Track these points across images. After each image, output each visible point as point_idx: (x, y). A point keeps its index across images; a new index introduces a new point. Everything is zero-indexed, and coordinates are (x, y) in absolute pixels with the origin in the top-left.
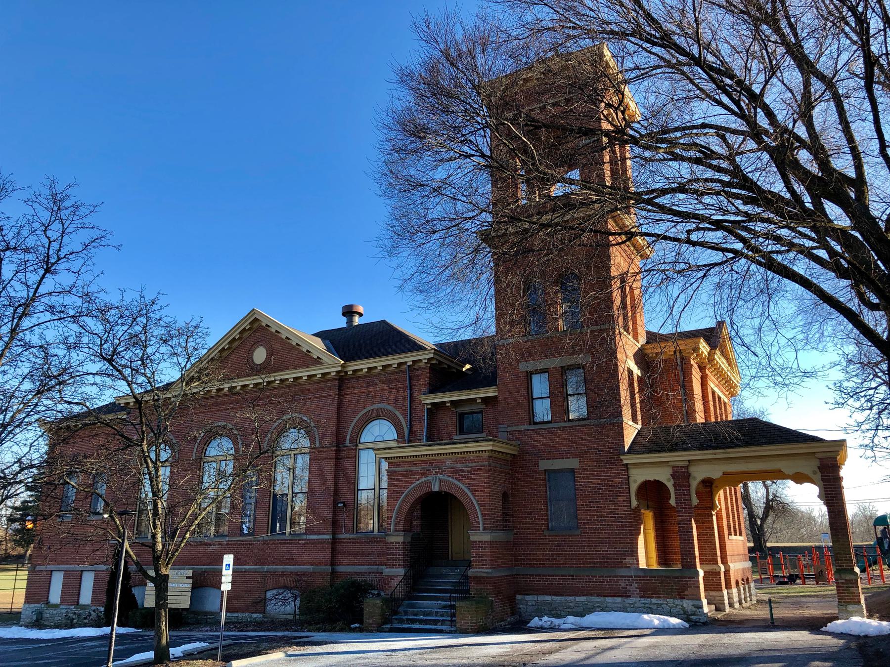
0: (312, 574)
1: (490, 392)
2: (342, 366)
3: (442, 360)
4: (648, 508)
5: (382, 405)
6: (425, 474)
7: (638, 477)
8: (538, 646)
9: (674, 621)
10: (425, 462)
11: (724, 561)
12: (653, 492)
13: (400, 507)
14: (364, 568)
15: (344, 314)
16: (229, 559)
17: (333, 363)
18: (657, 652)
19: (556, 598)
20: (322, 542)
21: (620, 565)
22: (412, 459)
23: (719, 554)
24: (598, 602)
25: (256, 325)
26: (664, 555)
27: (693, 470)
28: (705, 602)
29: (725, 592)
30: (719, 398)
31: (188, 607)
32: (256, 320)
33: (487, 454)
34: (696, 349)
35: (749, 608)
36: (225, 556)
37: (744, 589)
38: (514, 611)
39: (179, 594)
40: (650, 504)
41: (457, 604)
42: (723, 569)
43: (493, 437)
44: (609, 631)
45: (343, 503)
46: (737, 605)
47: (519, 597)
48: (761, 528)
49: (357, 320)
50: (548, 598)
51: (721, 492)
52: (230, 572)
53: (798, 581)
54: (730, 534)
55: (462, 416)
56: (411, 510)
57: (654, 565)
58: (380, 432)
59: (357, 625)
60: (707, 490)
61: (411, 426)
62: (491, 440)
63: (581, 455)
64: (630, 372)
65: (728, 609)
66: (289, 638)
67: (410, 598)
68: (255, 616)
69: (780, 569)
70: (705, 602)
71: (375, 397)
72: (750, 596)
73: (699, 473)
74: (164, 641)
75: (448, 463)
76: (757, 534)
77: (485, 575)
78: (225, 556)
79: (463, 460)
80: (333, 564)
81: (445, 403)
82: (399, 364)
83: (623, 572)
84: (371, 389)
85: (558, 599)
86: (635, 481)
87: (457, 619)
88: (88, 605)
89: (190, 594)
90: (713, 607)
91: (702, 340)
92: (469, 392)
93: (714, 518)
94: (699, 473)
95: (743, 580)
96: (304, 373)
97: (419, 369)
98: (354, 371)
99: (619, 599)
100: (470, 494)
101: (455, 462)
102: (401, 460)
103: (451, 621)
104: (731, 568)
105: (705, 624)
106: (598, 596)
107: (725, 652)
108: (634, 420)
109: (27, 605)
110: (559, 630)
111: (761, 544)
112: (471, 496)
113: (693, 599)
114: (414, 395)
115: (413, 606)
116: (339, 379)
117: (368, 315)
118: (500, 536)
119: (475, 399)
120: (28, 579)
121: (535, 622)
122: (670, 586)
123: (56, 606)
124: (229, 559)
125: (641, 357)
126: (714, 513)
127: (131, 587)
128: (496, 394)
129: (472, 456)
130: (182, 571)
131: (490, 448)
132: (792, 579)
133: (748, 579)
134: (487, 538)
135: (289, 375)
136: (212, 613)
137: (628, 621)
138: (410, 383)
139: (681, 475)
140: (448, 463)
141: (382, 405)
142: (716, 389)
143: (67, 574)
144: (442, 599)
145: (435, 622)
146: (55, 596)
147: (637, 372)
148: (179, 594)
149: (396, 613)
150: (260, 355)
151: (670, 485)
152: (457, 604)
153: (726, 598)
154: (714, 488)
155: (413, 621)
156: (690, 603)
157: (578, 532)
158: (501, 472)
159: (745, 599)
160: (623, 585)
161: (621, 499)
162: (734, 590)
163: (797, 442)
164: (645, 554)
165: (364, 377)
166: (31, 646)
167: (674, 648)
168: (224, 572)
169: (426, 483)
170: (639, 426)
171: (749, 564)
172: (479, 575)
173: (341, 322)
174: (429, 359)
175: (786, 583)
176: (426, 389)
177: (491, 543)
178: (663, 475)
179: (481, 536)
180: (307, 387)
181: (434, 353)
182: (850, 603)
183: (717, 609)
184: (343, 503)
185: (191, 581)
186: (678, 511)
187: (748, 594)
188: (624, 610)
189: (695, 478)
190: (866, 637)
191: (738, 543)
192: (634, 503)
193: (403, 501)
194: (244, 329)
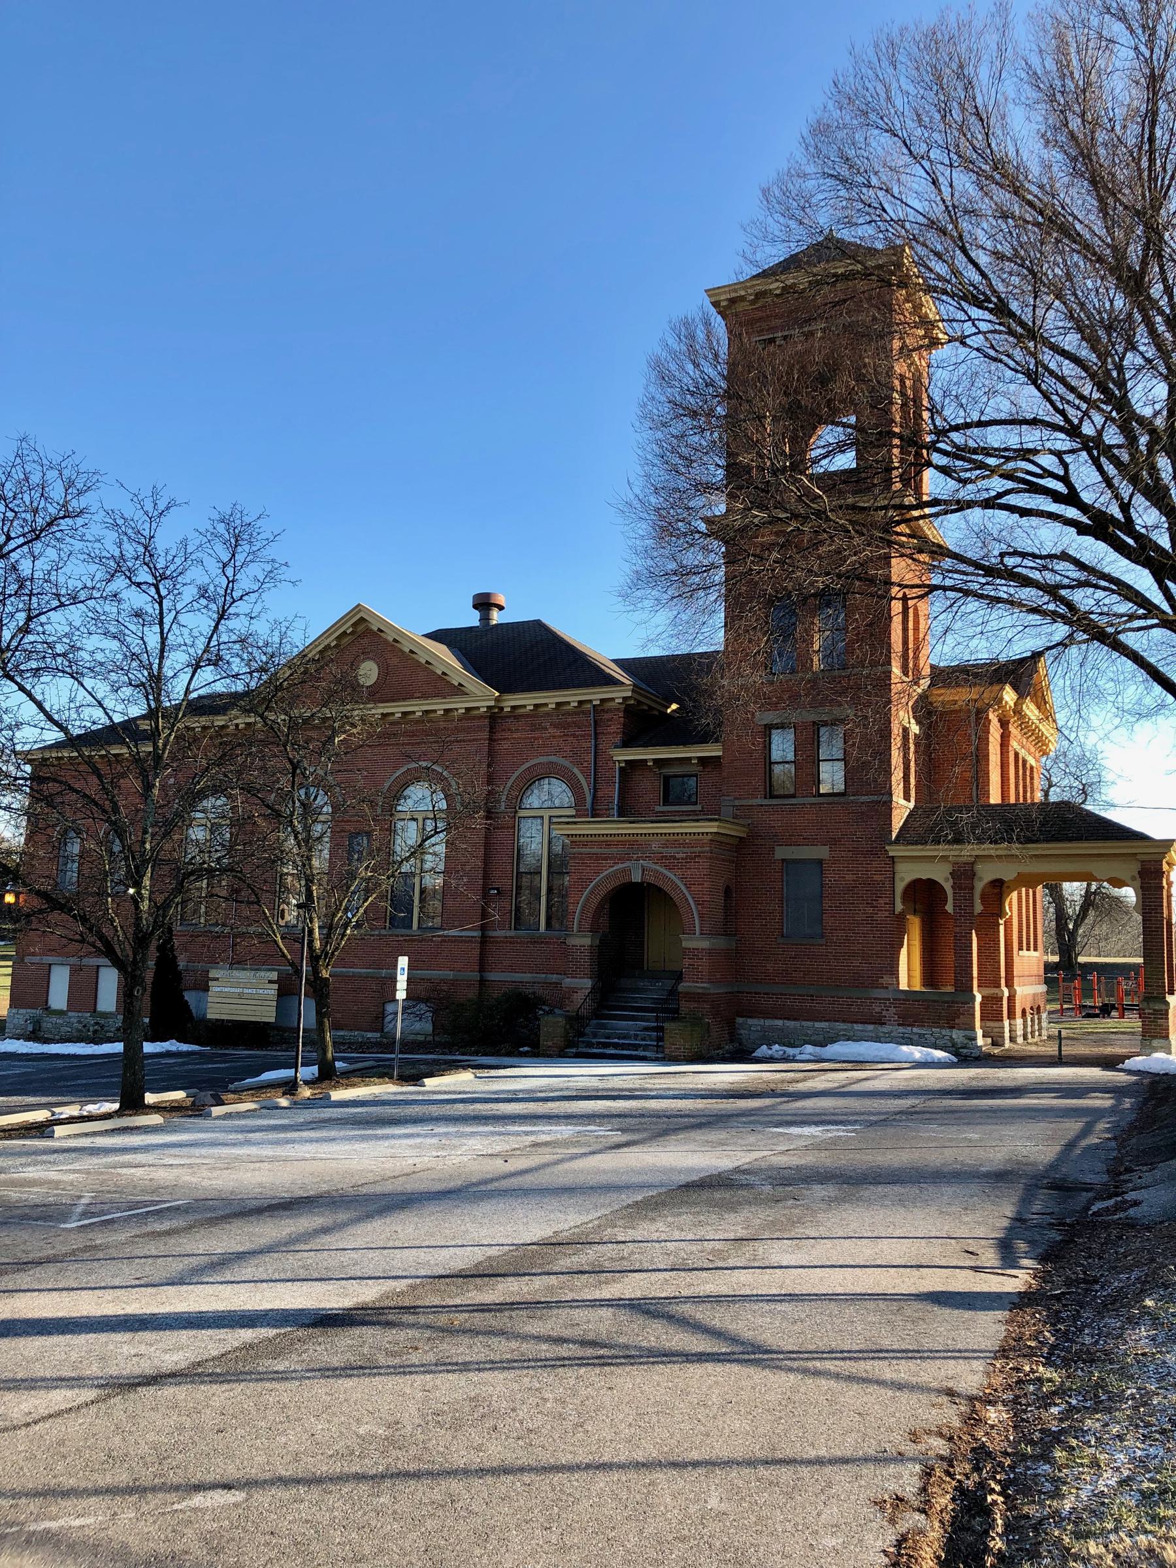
0: (454, 983)
1: (712, 750)
2: (497, 700)
3: (653, 705)
4: (915, 912)
5: (553, 759)
6: (622, 860)
7: (907, 874)
8: (779, 1076)
9: (939, 1054)
10: (623, 843)
11: (1010, 984)
12: (924, 895)
13: (587, 900)
14: (527, 977)
15: (475, 607)
16: (403, 962)
17: (481, 695)
18: (922, 1083)
19: (788, 1023)
20: (470, 940)
21: (876, 985)
22: (605, 838)
23: (1003, 974)
24: (845, 1030)
25: (361, 628)
26: (931, 974)
27: (979, 867)
28: (979, 1033)
29: (1006, 1023)
30: (1025, 762)
31: (273, 1020)
32: (362, 620)
33: (710, 837)
34: (999, 700)
35: (1036, 1044)
36: (400, 958)
37: (1032, 1020)
38: (733, 1036)
39: (259, 1003)
40: (918, 906)
41: (666, 1025)
42: (1006, 994)
43: (710, 813)
44: (858, 1063)
45: (497, 889)
46: (1020, 1040)
47: (740, 1020)
48: (1072, 934)
49: (496, 617)
50: (779, 1023)
51: (1015, 895)
52: (405, 977)
53: (1114, 1013)
54: (1021, 949)
55: (667, 779)
56: (600, 906)
57: (917, 987)
58: (550, 796)
59: (526, 1049)
60: (996, 891)
61: (595, 790)
62: (716, 820)
63: (833, 842)
64: (906, 730)
65: (1007, 1044)
66: (455, 1061)
67: (599, 1017)
68: (369, 1035)
69: (1092, 997)
70: (979, 1033)
71: (544, 746)
72: (1040, 1029)
73: (986, 874)
74: (329, 1055)
75: (655, 847)
76: (1065, 942)
77: (700, 991)
78: (400, 958)
79: (671, 845)
80: (482, 969)
81: (646, 761)
82: (581, 703)
83: (881, 994)
84: (537, 734)
85: (791, 1024)
86: (902, 879)
87: (666, 1044)
88: (111, 1013)
89: (275, 1003)
90: (989, 1040)
91: (1008, 688)
92: (681, 748)
93: (1002, 928)
94: (986, 874)
95: (1032, 1008)
96: (438, 706)
97: (609, 711)
98: (514, 708)
99: (871, 1027)
100: (683, 888)
101: (665, 846)
102: (590, 838)
103: (657, 1046)
104: (1018, 993)
105: (977, 1059)
106: (844, 1021)
107: (999, 1084)
108: (907, 797)
109: (14, 1011)
110: (793, 1060)
111: (1070, 957)
112: (685, 891)
113: (965, 1029)
114: (601, 747)
115: (604, 1027)
116: (490, 717)
117: (512, 611)
118: (721, 943)
119: (690, 759)
120: (12, 975)
121: (763, 1051)
122: (937, 1013)
123: (60, 1013)
124: (403, 962)
125: (924, 709)
126: (1001, 922)
127: (182, 991)
128: (720, 754)
129: (688, 839)
130: (262, 974)
131: (715, 830)
132: (1106, 1011)
133: (1039, 1008)
134: (705, 944)
135: (418, 707)
136: (291, 1029)
137: (882, 1053)
138: (595, 730)
139: (964, 875)
140: (655, 847)
141: (553, 759)
142: (1023, 753)
143: (75, 971)
144: (642, 1019)
145: (636, 1047)
146: (58, 997)
147: (915, 729)
148: (259, 1003)
149: (582, 1034)
150: (369, 672)
151: (948, 886)
152: (666, 1025)
153: (1007, 1030)
154: (1004, 888)
155: (606, 1045)
156: (961, 1033)
157: (823, 941)
158: (723, 860)
159: (1032, 1032)
160: (878, 1009)
161: (881, 901)
162: (1019, 1021)
163: (1117, 839)
164: (908, 971)
165: (527, 716)
166: (89, 1062)
167: (949, 1079)
168: (399, 977)
169: (624, 870)
170: (912, 805)
171: (1043, 988)
172: (692, 990)
173: (472, 619)
174: (624, 698)
175: (1097, 1016)
176: (618, 739)
177: (710, 952)
178: (940, 874)
179: (697, 942)
180: (442, 724)
181: (633, 691)
182: (1155, 1037)
183: (994, 1044)
184: (497, 889)
185: (276, 986)
186: (955, 920)
187: (1036, 1027)
188: (877, 1039)
189: (981, 879)
190: (1166, 1074)
191: (1030, 963)
192: (899, 907)
193: (592, 892)
194: (345, 632)
